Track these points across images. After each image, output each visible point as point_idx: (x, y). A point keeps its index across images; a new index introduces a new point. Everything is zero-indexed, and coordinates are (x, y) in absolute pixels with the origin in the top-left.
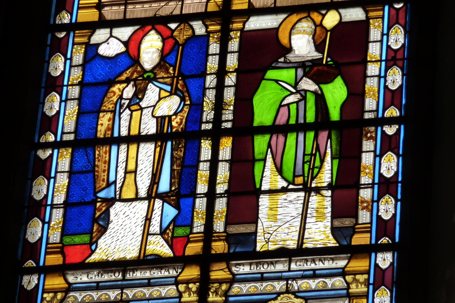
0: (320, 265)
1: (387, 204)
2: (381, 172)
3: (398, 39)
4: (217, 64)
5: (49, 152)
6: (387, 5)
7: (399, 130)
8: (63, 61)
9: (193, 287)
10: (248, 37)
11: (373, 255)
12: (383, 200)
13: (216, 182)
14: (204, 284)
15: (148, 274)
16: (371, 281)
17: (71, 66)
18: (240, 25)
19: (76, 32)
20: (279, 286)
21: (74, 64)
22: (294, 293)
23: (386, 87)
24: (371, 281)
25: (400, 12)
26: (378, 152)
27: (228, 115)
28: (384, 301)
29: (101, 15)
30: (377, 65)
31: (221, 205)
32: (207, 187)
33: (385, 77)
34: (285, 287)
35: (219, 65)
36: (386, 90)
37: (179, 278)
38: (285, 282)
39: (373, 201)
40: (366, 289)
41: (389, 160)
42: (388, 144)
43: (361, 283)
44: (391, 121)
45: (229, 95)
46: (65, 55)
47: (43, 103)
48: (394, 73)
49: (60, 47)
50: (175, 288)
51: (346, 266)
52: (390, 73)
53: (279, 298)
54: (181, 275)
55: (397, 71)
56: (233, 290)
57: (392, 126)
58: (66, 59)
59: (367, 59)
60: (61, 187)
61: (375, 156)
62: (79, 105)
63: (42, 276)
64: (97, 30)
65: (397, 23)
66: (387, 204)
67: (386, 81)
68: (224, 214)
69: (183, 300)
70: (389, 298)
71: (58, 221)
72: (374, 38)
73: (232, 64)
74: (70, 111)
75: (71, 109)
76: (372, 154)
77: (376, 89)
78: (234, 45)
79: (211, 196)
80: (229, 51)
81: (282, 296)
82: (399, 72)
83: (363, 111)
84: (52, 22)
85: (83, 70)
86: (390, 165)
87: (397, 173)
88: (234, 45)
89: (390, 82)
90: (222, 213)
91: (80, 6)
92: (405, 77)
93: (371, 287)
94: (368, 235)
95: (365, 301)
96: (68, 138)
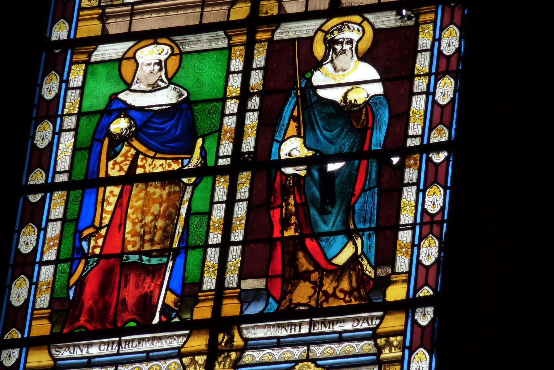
0: (348, 326)
3: (451, 41)
5: (39, 196)
7: (447, 159)
8: (28, 286)
9: (201, 359)
10: (275, 48)
12: (447, 33)
14: (213, 353)
15: (146, 346)
16: (408, 343)
17: (67, 89)
18: (268, 35)
20: (298, 352)
21: (71, 86)
22: (314, 361)
23: (419, 262)
24: (408, 343)
26: (422, 187)
28: (422, 368)
29: (104, 29)
30: (425, 80)
31: (235, 253)
32: (220, 236)
33: (419, 246)
34: (304, 354)
36: (430, 163)
37: (379, 330)
38: (306, 348)
39: (413, 245)
40: (401, 354)
42: (433, 176)
43: (395, 347)
44: (438, 147)
46: (61, 76)
47: (41, 86)
48: (420, 359)
49: (58, 67)
50: (179, 362)
51: (182, 346)
52: (424, 243)
53: (297, 367)
54: (185, 346)
55: (454, 32)
56: (244, 360)
57: (441, 153)
58: (31, 284)
59: (414, 72)
61: (418, 191)
62: (76, 137)
63: (24, 349)
64: (99, 46)
65: (452, 23)
67: (440, 45)
68: (244, 221)
69: (382, 356)
70: (442, 197)
73: (234, 260)
74: (70, 104)
75: (77, 76)
76: (415, 188)
77: (422, 111)
78: (259, 60)
79: (225, 246)
81: (300, 364)
82: (451, 83)
83: (406, 136)
84: (24, 183)
86: (436, 200)
87: (443, 209)
88: (259, 60)
89: (445, 45)
90: (240, 220)
91: (80, 18)
92: (457, 94)
93: (407, 352)
95: (398, 368)
96: (61, 178)
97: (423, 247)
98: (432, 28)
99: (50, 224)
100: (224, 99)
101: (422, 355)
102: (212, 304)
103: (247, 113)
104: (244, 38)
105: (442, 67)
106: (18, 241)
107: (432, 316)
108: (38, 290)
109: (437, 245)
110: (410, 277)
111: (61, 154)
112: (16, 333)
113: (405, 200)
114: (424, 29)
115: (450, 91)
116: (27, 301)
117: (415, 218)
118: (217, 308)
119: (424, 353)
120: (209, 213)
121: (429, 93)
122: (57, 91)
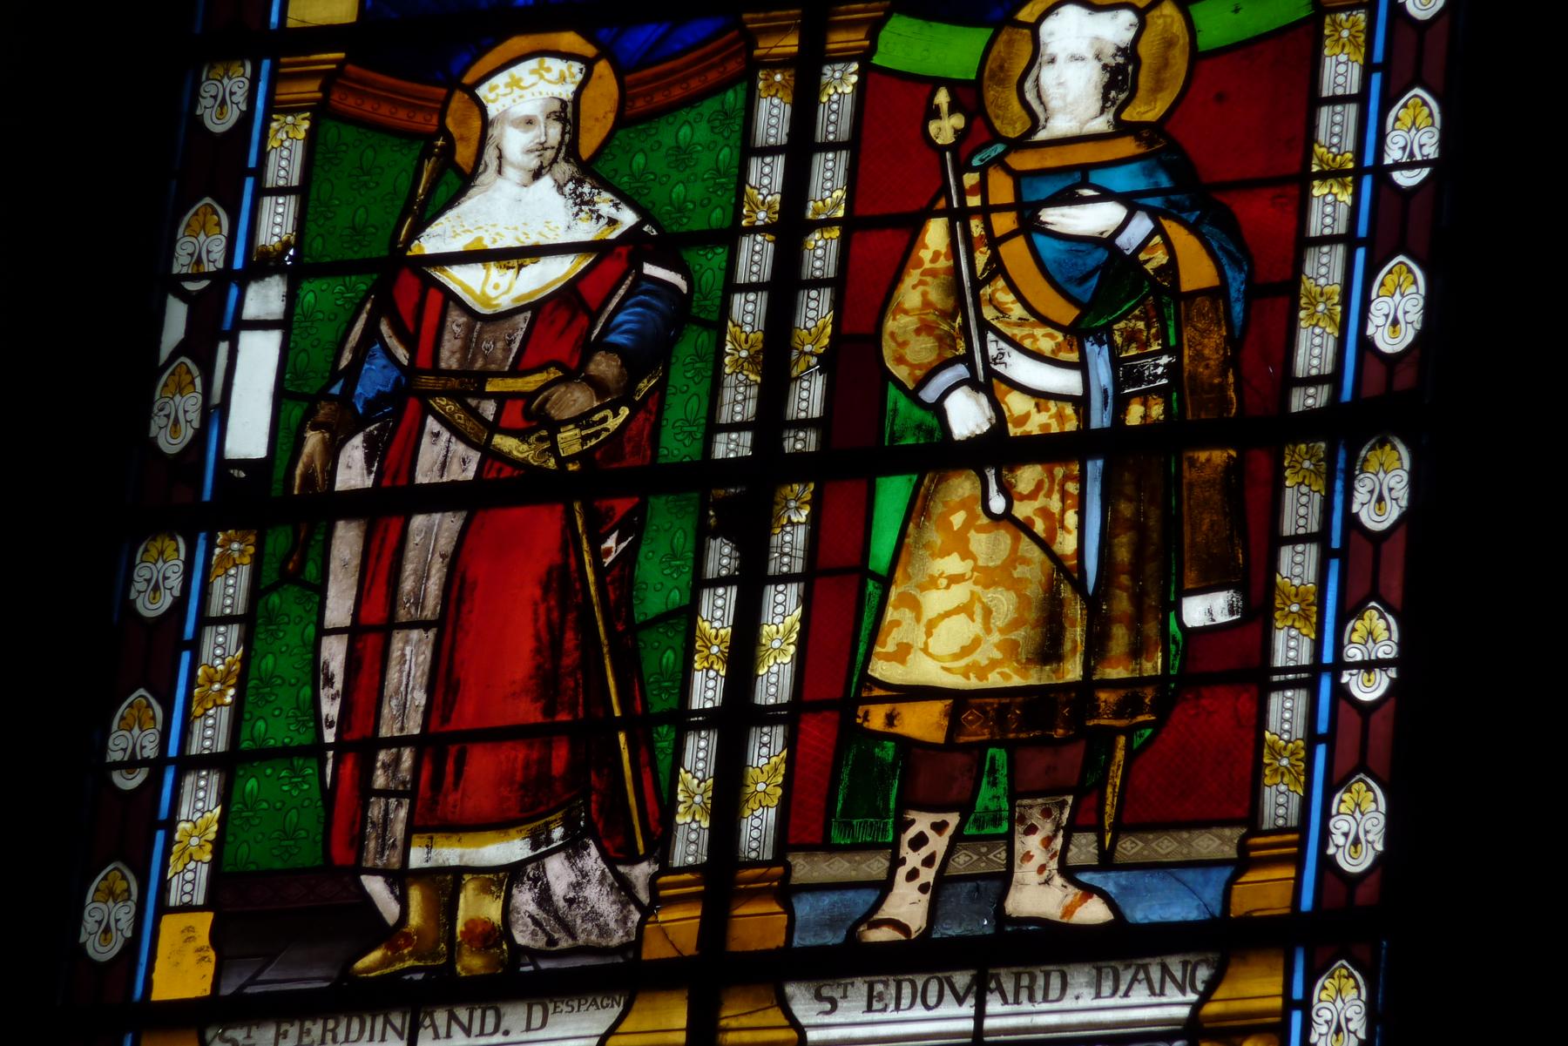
1: (1370, 642)
2: (1370, 331)
4: (762, 327)
6: (1307, 914)
11: (1307, 902)
13: (789, 371)
19: (284, 60)
25: (1375, 718)
27: (808, 397)
35: (735, 627)
41: (1358, 805)
45: (815, 314)
55: (1426, 111)
60: (196, 833)
66: (1370, 642)
71: (221, 667)
72: (1311, 366)
76: (1312, 551)
80: (819, 138)
83: (1290, 381)
85: (247, 641)
89: (1381, 321)
94: (1289, 872)
97: (1351, 642)
98: (1362, 25)
99: (209, 632)
100: (729, 237)
101: (1363, 794)
102: (698, 913)
103: (754, 733)
104: (790, 44)
105: (1388, 227)
106: (129, 581)
107: (1380, 847)
108: (175, 848)
109: (1422, 290)
110: (1302, 844)
111: (277, 131)
112: (124, 877)
113: (1324, 150)
114: (1337, 26)
115: (1356, 1018)
116: (180, 604)
117: (1318, 645)
118: (715, 926)
119: (1425, 103)
120: (690, 611)
121: (1322, 671)
122: (244, 107)
